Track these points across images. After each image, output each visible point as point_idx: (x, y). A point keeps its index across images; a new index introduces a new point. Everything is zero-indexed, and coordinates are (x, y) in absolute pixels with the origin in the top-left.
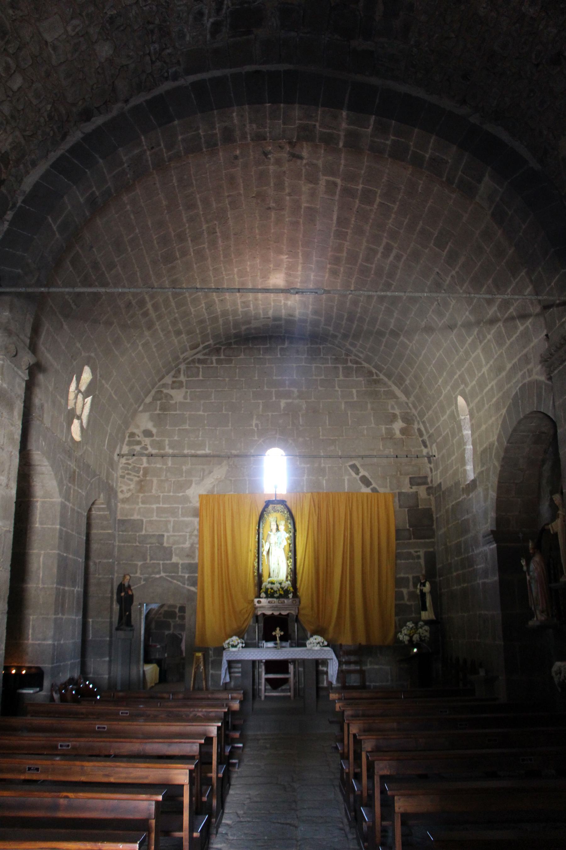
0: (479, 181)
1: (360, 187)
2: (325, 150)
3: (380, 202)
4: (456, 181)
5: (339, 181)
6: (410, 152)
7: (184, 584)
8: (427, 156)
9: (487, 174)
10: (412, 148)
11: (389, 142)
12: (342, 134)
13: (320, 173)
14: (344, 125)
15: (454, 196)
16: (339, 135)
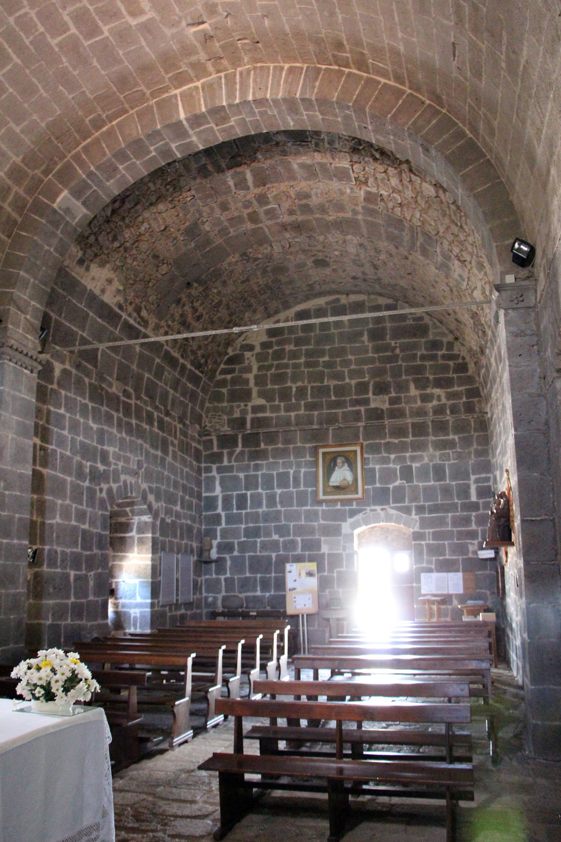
0: (84, 203)
1: (106, 29)
2: (173, 50)
3: (69, 29)
4: (89, 181)
5: (133, 22)
6: (132, 156)
7: (505, 77)
8: (121, 167)
9: (88, 213)
10: (134, 160)
11: (152, 148)
12: (191, 132)
13: (158, 18)
14: (194, 139)
15: (43, 125)
16: (193, 129)
